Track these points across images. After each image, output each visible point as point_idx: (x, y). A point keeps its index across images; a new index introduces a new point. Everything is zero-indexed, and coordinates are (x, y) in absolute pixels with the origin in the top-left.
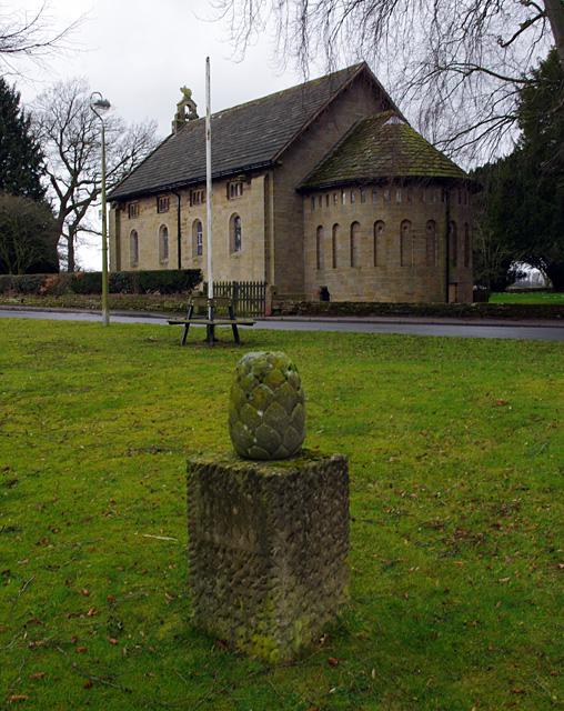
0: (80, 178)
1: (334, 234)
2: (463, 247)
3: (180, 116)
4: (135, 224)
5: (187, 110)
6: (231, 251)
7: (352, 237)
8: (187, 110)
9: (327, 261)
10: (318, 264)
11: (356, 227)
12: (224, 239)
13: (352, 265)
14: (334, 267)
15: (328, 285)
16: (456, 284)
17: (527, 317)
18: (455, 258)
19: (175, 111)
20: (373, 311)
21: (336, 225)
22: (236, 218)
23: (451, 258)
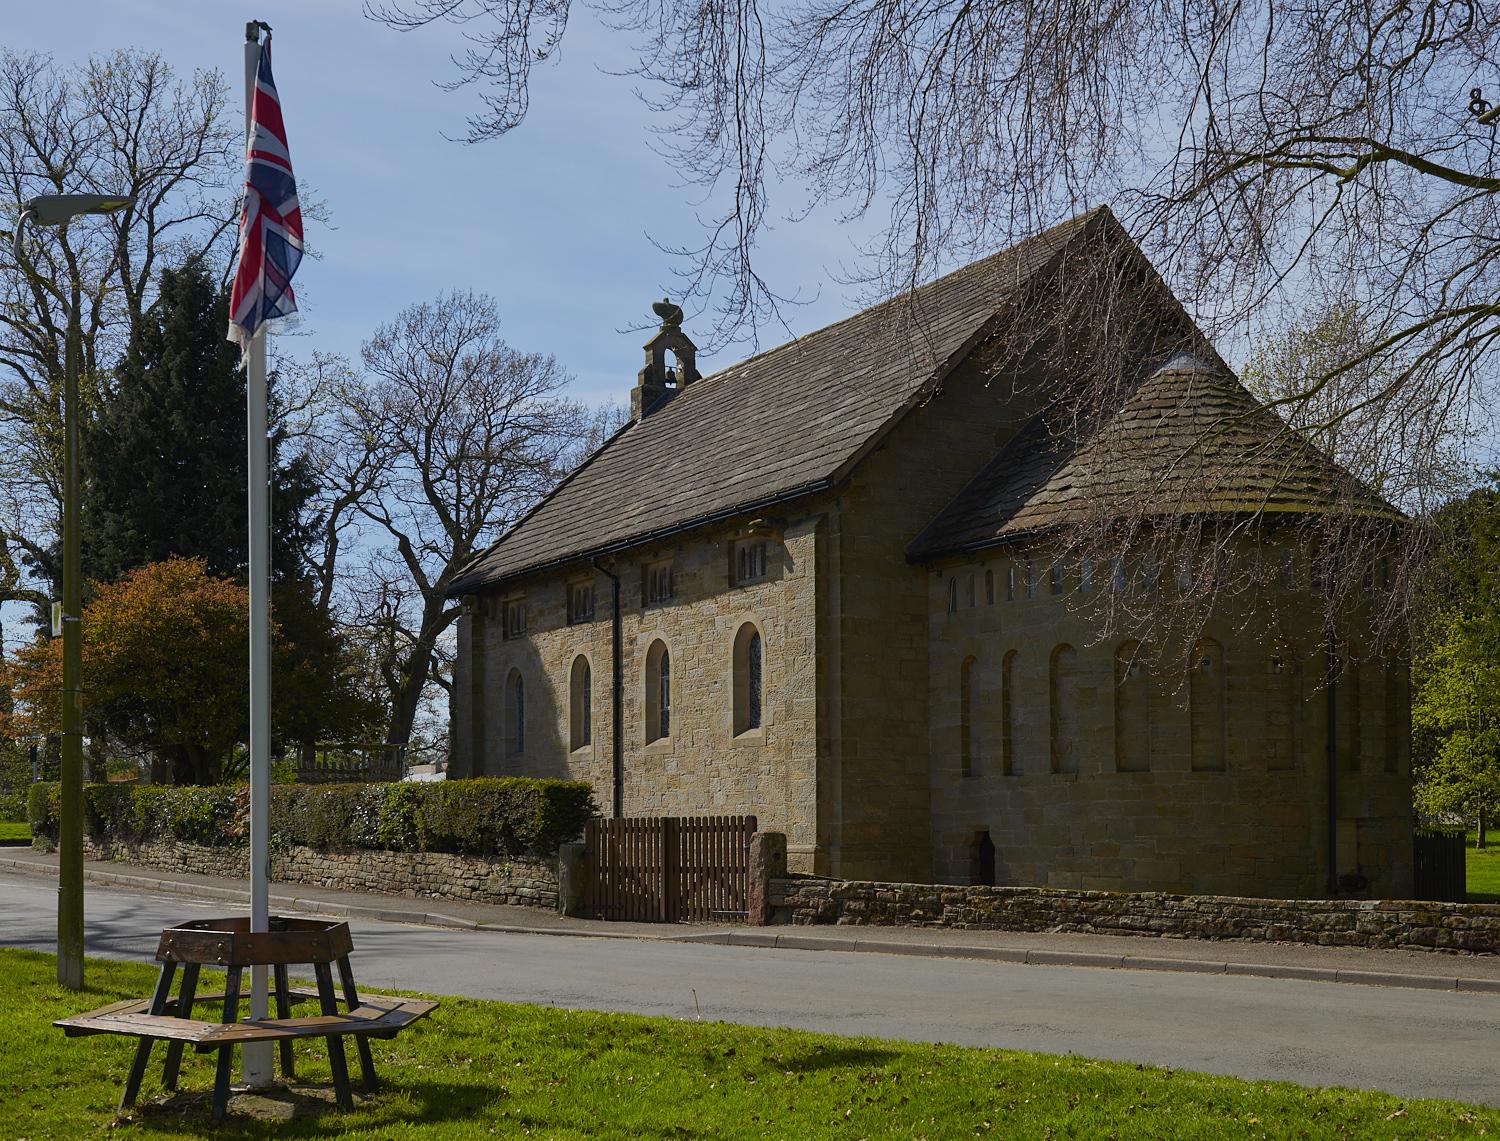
5: (671, 359)
6: (739, 729)
7: (1054, 685)
8: (671, 359)
10: (966, 761)
13: (1056, 770)
14: (1008, 771)
19: (641, 361)
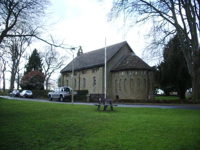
0: (50, 66)
1: (120, 82)
2: (152, 86)
3: (79, 52)
4: (68, 78)
9: (118, 88)
11: (126, 80)
12: (95, 83)
14: (120, 90)
15: (118, 95)
16: (150, 94)
17: (126, 102)
18: (150, 88)
20: (138, 102)
21: (121, 80)
22: (94, 77)
23: (149, 88)
